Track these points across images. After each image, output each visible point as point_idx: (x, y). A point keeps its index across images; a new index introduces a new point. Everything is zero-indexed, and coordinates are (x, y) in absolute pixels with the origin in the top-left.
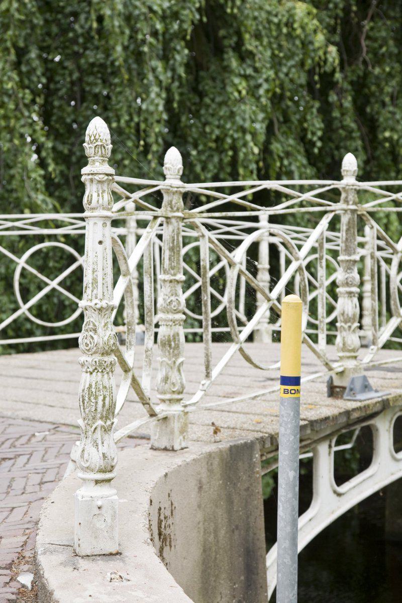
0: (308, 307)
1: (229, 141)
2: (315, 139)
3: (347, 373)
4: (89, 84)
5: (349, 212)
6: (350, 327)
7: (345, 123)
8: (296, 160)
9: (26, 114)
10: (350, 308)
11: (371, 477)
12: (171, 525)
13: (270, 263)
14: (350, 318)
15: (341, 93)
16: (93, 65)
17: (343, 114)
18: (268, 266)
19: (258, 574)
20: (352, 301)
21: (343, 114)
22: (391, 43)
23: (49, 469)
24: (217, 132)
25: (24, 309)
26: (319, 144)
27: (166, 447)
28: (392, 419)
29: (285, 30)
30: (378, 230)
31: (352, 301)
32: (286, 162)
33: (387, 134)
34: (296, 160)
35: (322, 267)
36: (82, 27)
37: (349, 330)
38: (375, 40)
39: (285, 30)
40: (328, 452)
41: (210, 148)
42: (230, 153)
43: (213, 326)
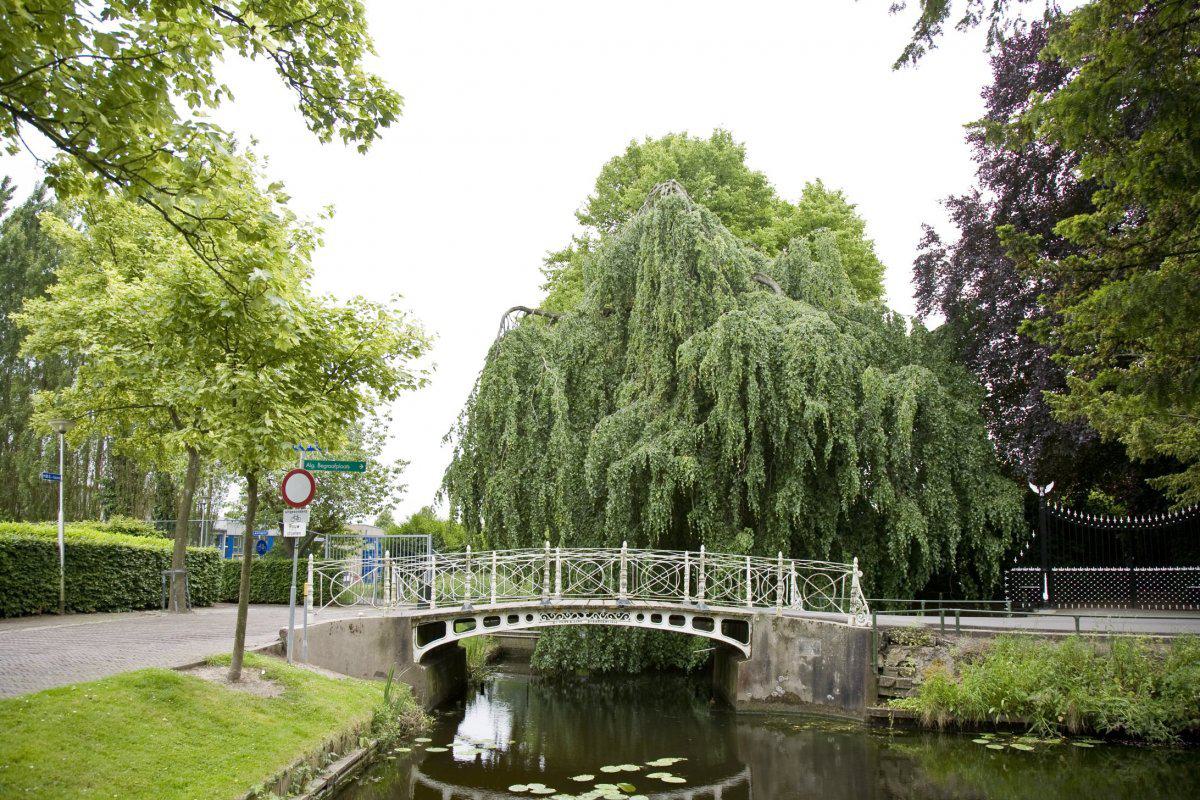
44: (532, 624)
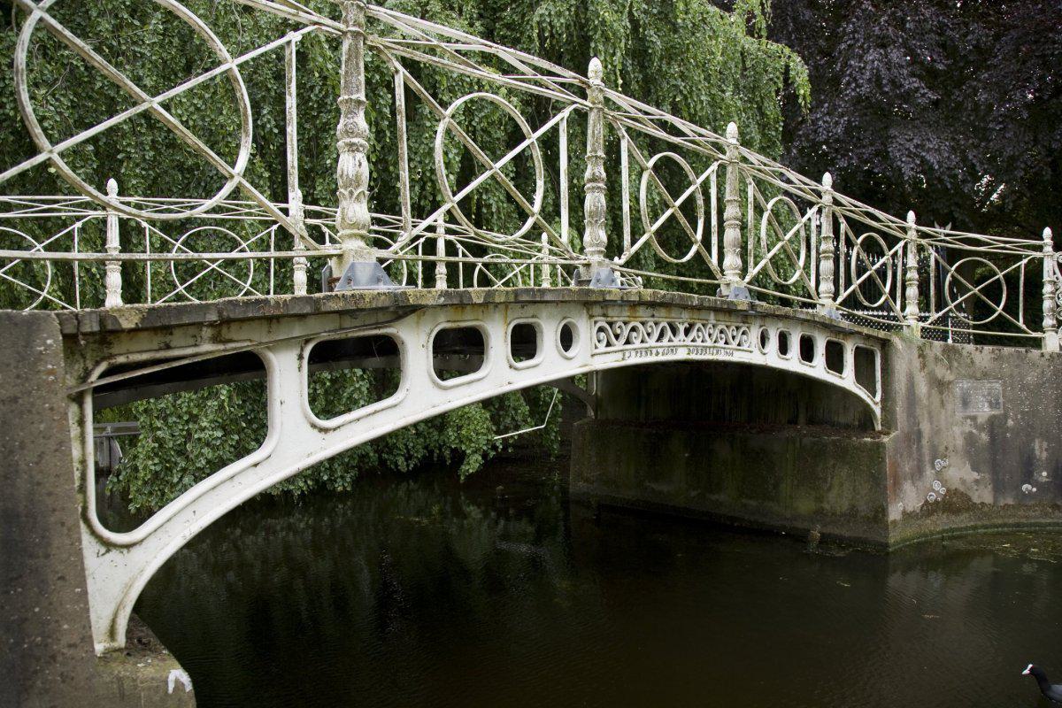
0: (367, 199)
3: (346, 256)
5: (349, 35)
6: (351, 193)
8: (495, 195)
10: (351, 165)
11: (479, 380)
12: (597, 344)
14: (351, 180)
19: (47, 556)
20: (354, 157)
27: (278, 322)
28: (432, 331)
30: (404, 75)
31: (354, 157)
32: (484, 197)
34: (495, 195)
35: (290, 95)
37: (351, 197)
40: (425, 356)
43: (472, 286)
44: (550, 365)
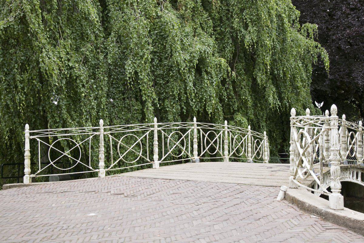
1: (205, 99)
2: (225, 98)
4: (158, 80)
7: (231, 94)
9: (150, 89)
13: (158, 138)
15: (229, 84)
16: (159, 74)
17: (230, 91)
18: (157, 139)
21: (230, 91)
22: (243, 70)
23: (214, 225)
24: (201, 96)
25: (121, 157)
26: (226, 100)
29: (218, 66)
33: (244, 97)
36: (155, 63)
38: (238, 69)
39: (218, 66)
41: (198, 101)
42: (204, 103)
